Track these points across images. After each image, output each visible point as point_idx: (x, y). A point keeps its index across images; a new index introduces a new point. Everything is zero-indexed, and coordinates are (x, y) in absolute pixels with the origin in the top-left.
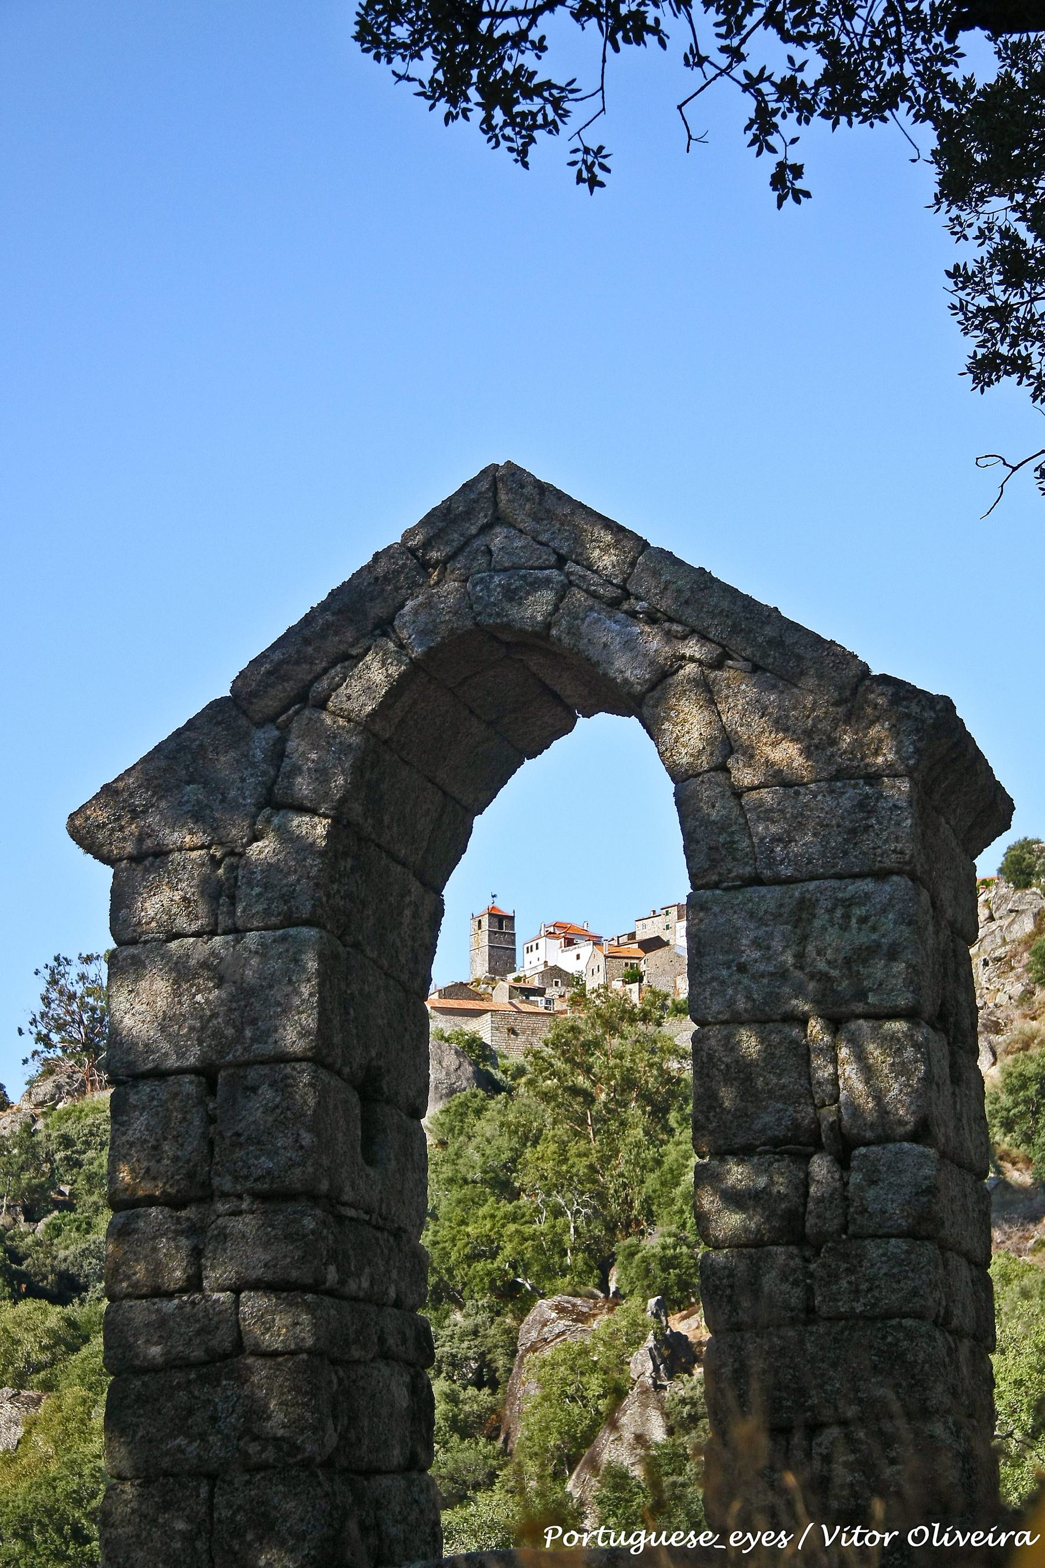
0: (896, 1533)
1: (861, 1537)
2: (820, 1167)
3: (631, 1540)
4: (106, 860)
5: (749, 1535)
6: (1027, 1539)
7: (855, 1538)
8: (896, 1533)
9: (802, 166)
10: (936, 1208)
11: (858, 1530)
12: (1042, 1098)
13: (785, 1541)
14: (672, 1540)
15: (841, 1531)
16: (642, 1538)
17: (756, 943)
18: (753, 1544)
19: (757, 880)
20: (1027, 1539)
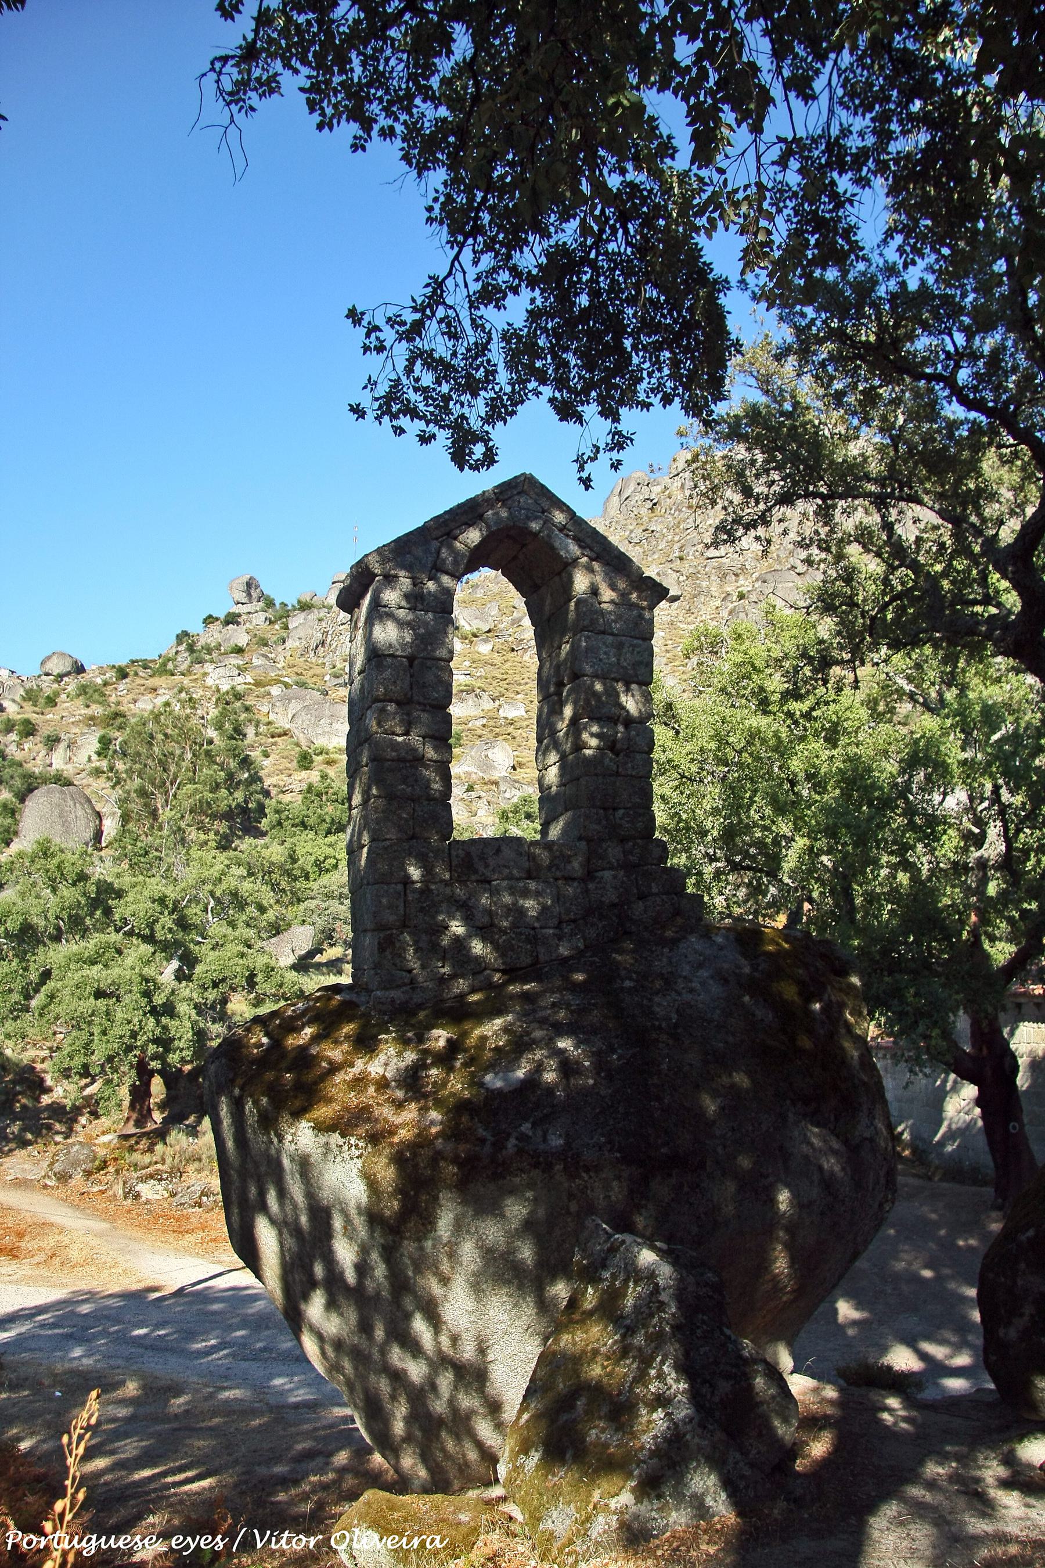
0: (1001, 67)
1: (289, 1541)
2: (621, 728)
3: (84, 1544)
4: (443, 606)
5: (189, 1539)
6: (437, 1542)
7: (283, 1541)
8: (1001, 67)
9: (664, 407)
10: (390, 1189)
11: (286, 1534)
12: (1026, 78)
13: (221, 1544)
14: (121, 1543)
15: (271, 1535)
16: (93, 1541)
17: (605, 653)
18: (193, 1546)
19: (603, 633)
20: (437, 1542)
